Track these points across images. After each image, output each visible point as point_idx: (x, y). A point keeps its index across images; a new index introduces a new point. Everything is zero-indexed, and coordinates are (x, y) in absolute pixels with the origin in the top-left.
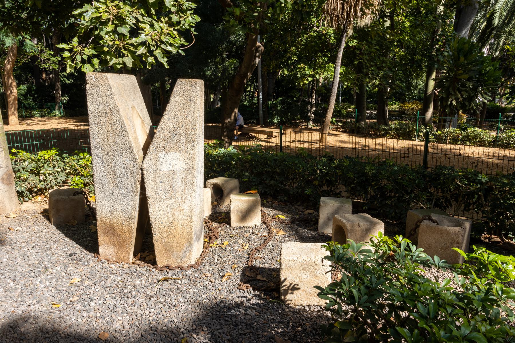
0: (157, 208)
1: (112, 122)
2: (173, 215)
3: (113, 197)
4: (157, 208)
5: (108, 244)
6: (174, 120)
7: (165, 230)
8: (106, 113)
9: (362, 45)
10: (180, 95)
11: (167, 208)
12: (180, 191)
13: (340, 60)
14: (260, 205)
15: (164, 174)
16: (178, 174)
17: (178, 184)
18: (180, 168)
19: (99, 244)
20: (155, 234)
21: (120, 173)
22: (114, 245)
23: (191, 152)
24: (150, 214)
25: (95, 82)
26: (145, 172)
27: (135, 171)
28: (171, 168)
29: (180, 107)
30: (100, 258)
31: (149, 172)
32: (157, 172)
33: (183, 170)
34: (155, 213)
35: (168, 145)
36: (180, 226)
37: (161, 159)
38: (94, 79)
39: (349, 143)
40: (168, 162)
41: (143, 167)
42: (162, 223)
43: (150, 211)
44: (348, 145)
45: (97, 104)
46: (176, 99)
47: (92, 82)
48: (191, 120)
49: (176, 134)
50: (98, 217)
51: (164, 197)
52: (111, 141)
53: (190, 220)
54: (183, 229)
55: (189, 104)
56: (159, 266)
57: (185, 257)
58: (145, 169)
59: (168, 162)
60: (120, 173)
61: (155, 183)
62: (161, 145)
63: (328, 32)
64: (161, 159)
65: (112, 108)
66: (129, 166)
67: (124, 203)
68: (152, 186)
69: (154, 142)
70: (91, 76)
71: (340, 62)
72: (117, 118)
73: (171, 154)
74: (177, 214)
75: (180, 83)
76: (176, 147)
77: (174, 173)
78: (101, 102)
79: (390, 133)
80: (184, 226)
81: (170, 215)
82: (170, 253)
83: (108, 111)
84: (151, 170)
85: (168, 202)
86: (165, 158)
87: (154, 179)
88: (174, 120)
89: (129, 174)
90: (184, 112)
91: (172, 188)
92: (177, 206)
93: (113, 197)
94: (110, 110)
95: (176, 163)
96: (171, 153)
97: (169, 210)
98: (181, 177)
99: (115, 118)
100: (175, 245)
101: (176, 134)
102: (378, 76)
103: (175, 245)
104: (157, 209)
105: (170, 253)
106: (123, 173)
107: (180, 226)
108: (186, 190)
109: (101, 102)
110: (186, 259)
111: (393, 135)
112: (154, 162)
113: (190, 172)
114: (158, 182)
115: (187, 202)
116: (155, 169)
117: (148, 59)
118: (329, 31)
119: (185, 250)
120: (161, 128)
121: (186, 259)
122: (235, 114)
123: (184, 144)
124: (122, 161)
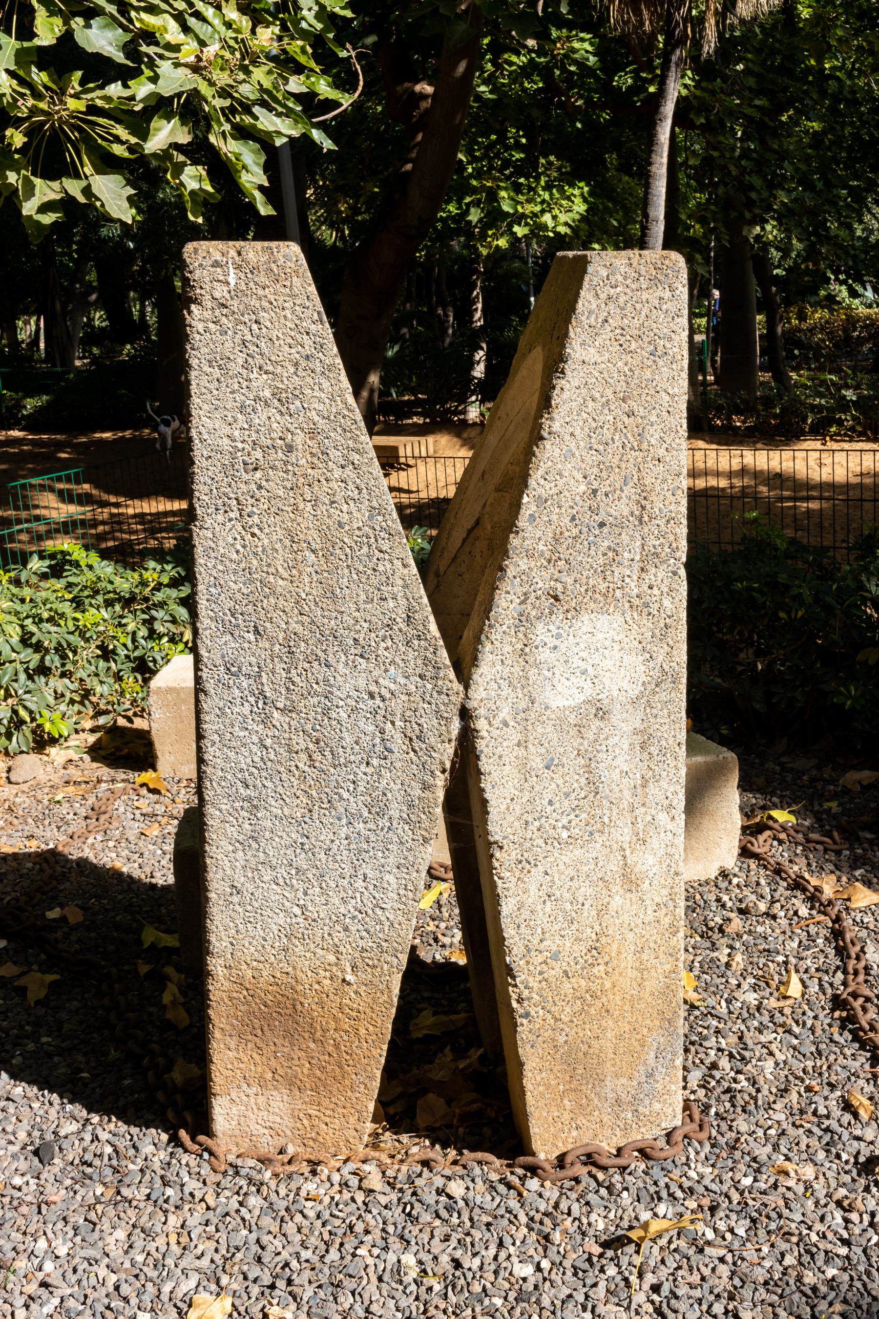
0: (533, 889)
1: (322, 491)
2: (602, 911)
3: (302, 861)
4: (533, 889)
5: (262, 1083)
6: (592, 458)
7: (567, 986)
8: (290, 448)
9: (713, 93)
10: (606, 334)
11: (575, 884)
12: (627, 794)
13: (665, 154)
14: (734, 778)
15: (560, 724)
16: (616, 718)
17: (619, 761)
18: (625, 685)
19: (216, 1089)
20: (527, 1015)
21: (349, 739)
22: (293, 1084)
23: (667, 603)
24: (505, 922)
25: (236, 293)
26: (481, 725)
27: (429, 722)
28: (589, 691)
29: (609, 392)
30: (220, 1151)
31: (496, 722)
32: (533, 716)
33: (634, 691)
34: (526, 914)
35: (570, 580)
36: (628, 960)
37: (544, 655)
38: (232, 280)
39: (718, 474)
40: (576, 662)
41: (471, 705)
42: (555, 957)
43: (507, 908)
44: (712, 482)
45: (242, 408)
46: (591, 355)
47: (220, 292)
48: (661, 452)
49: (602, 525)
50: (216, 965)
51: (565, 834)
52: (308, 588)
53: (667, 921)
54: (642, 970)
55: (648, 374)
56: (542, 1156)
57: (652, 1095)
58: (482, 711)
59: (576, 662)
60: (349, 739)
61: (526, 772)
62: (542, 582)
63: (574, 51)
64: (544, 655)
65: (321, 423)
66: (397, 705)
67: (359, 884)
68: (510, 790)
69: (511, 572)
70: (216, 264)
71: (665, 160)
72: (349, 471)
73: (585, 622)
74: (617, 902)
75: (604, 273)
76: (602, 587)
77: (602, 713)
78: (267, 393)
79: (840, 423)
80: (645, 957)
81: (589, 914)
82: (587, 1089)
83: (299, 439)
84: (505, 713)
85: (578, 852)
86: (563, 648)
87: (522, 752)
88: (592, 458)
89: (398, 742)
90: (630, 414)
91: (593, 785)
92: (614, 866)
93: (302, 861)
94: (313, 433)
95: (608, 664)
96: (585, 617)
97: (585, 890)
98: (627, 728)
99: (337, 473)
100: (609, 1047)
101: (602, 525)
102: (769, 208)
103: (609, 1047)
104: (533, 896)
105: (587, 1089)
106: (365, 740)
107: (628, 960)
108: (652, 789)
109: (267, 393)
110: (657, 1106)
111: (852, 429)
112: (517, 669)
113: (664, 696)
114: (537, 763)
115: (654, 842)
116: (523, 705)
117: (183, 177)
118: (576, 45)
119: (651, 1061)
120: (541, 501)
121: (657, 1106)
122: (372, 391)
123: (636, 566)
124: (361, 683)
